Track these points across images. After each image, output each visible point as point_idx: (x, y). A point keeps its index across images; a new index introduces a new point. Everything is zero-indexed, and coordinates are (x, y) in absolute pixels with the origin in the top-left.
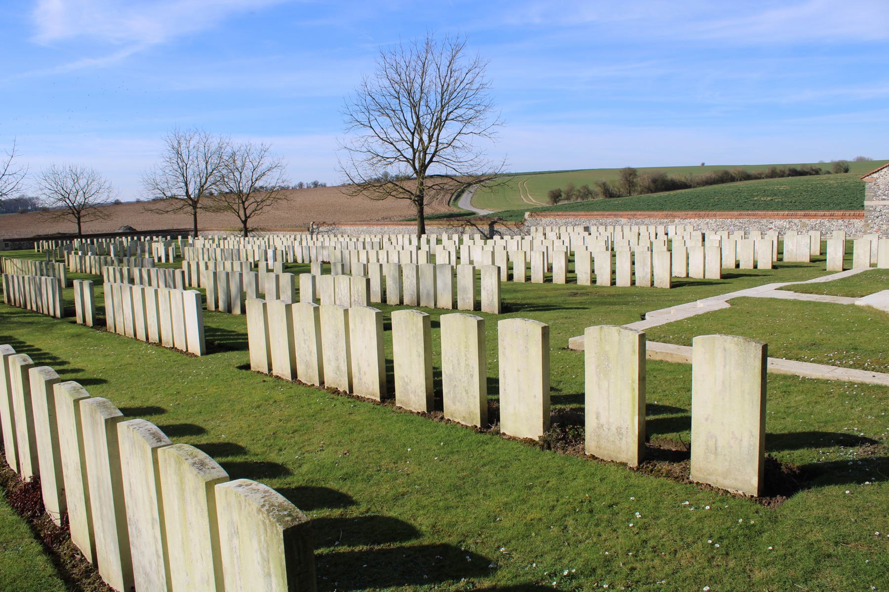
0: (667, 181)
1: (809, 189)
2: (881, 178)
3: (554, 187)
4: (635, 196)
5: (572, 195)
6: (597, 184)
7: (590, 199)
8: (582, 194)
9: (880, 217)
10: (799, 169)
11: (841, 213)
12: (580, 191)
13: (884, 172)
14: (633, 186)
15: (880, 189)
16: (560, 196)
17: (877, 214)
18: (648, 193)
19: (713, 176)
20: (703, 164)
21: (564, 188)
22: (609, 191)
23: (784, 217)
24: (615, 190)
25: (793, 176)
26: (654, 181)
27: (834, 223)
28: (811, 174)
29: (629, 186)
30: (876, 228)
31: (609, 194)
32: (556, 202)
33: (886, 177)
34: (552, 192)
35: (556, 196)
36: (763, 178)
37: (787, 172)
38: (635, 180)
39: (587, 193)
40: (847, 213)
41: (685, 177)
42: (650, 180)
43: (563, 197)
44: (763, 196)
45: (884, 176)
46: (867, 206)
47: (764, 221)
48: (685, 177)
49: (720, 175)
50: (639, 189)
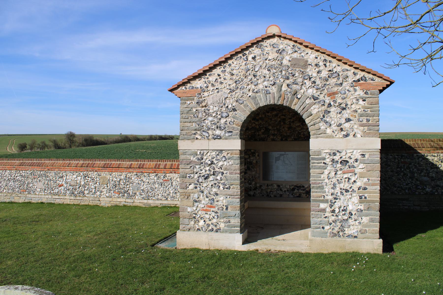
0: (94, 140)
1: (166, 146)
2: (210, 88)
3: (22, 142)
4: (74, 148)
5: (34, 147)
6: (50, 141)
7: (46, 149)
8: (41, 146)
9: (211, 178)
10: (163, 137)
11: (153, 164)
12: (39, 145)
13: (216, 77)
14: (73, 143)
15: (209, 115)
16: (26, 147)
17: (205, 170)
18: (82, 147)
19: (120, 138)
20: (121, 134)
21: (28, 142)
22: (57, 145)
23: (77, 169)
24: (62, 145)
25: (161, 140)
26: (86, 140)
27: (144, 180)
28: (169, 139)
29: (70, 143)
30: (205, 201)
31: (57, 146)
32: (22, 150)
33: (220, 86)
34: (20, 144)
35: (23, 147)
36: (146, 141)
37: (158, 138)
38: (74, 139)
39: (44, 146)
40: (162, 164)
41: (104, 139)
42: (83, 139)
43: (28, 148)
44: (142, 149)
45: (217, 85)
46: (184, 154)
47: (51, 174)
48: (104, 139)
49: (123, 138)
50: (77, 144)
